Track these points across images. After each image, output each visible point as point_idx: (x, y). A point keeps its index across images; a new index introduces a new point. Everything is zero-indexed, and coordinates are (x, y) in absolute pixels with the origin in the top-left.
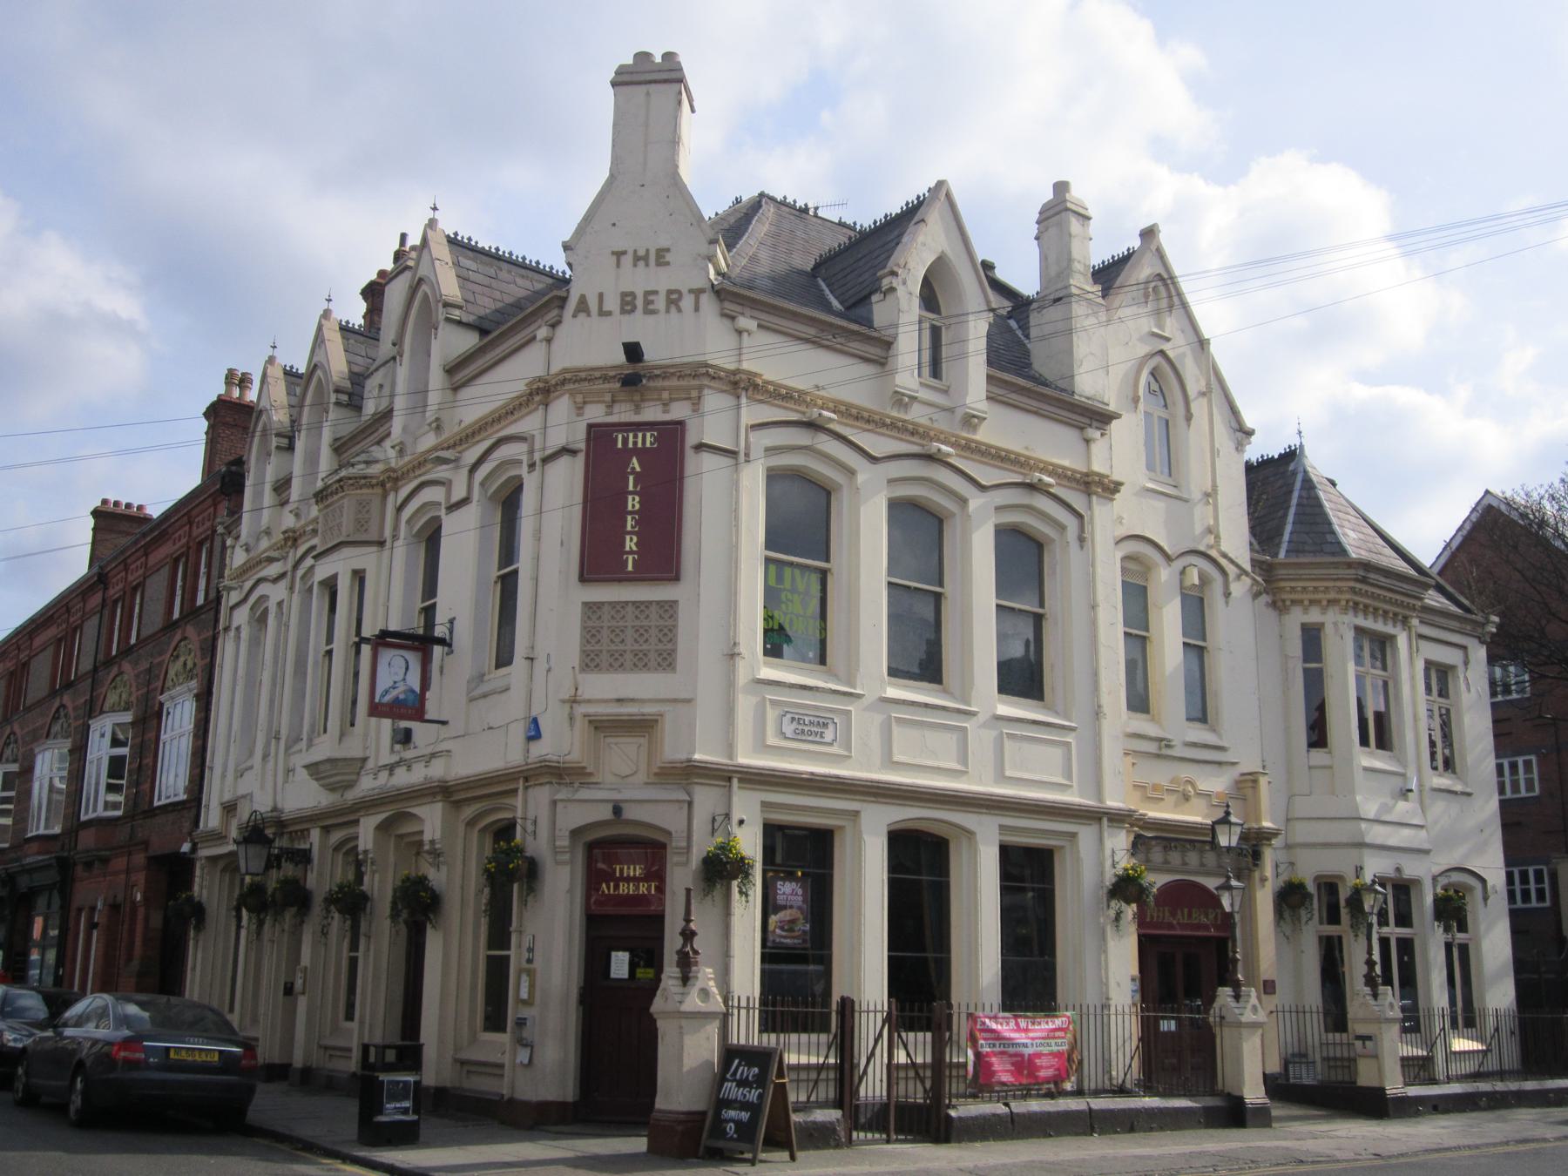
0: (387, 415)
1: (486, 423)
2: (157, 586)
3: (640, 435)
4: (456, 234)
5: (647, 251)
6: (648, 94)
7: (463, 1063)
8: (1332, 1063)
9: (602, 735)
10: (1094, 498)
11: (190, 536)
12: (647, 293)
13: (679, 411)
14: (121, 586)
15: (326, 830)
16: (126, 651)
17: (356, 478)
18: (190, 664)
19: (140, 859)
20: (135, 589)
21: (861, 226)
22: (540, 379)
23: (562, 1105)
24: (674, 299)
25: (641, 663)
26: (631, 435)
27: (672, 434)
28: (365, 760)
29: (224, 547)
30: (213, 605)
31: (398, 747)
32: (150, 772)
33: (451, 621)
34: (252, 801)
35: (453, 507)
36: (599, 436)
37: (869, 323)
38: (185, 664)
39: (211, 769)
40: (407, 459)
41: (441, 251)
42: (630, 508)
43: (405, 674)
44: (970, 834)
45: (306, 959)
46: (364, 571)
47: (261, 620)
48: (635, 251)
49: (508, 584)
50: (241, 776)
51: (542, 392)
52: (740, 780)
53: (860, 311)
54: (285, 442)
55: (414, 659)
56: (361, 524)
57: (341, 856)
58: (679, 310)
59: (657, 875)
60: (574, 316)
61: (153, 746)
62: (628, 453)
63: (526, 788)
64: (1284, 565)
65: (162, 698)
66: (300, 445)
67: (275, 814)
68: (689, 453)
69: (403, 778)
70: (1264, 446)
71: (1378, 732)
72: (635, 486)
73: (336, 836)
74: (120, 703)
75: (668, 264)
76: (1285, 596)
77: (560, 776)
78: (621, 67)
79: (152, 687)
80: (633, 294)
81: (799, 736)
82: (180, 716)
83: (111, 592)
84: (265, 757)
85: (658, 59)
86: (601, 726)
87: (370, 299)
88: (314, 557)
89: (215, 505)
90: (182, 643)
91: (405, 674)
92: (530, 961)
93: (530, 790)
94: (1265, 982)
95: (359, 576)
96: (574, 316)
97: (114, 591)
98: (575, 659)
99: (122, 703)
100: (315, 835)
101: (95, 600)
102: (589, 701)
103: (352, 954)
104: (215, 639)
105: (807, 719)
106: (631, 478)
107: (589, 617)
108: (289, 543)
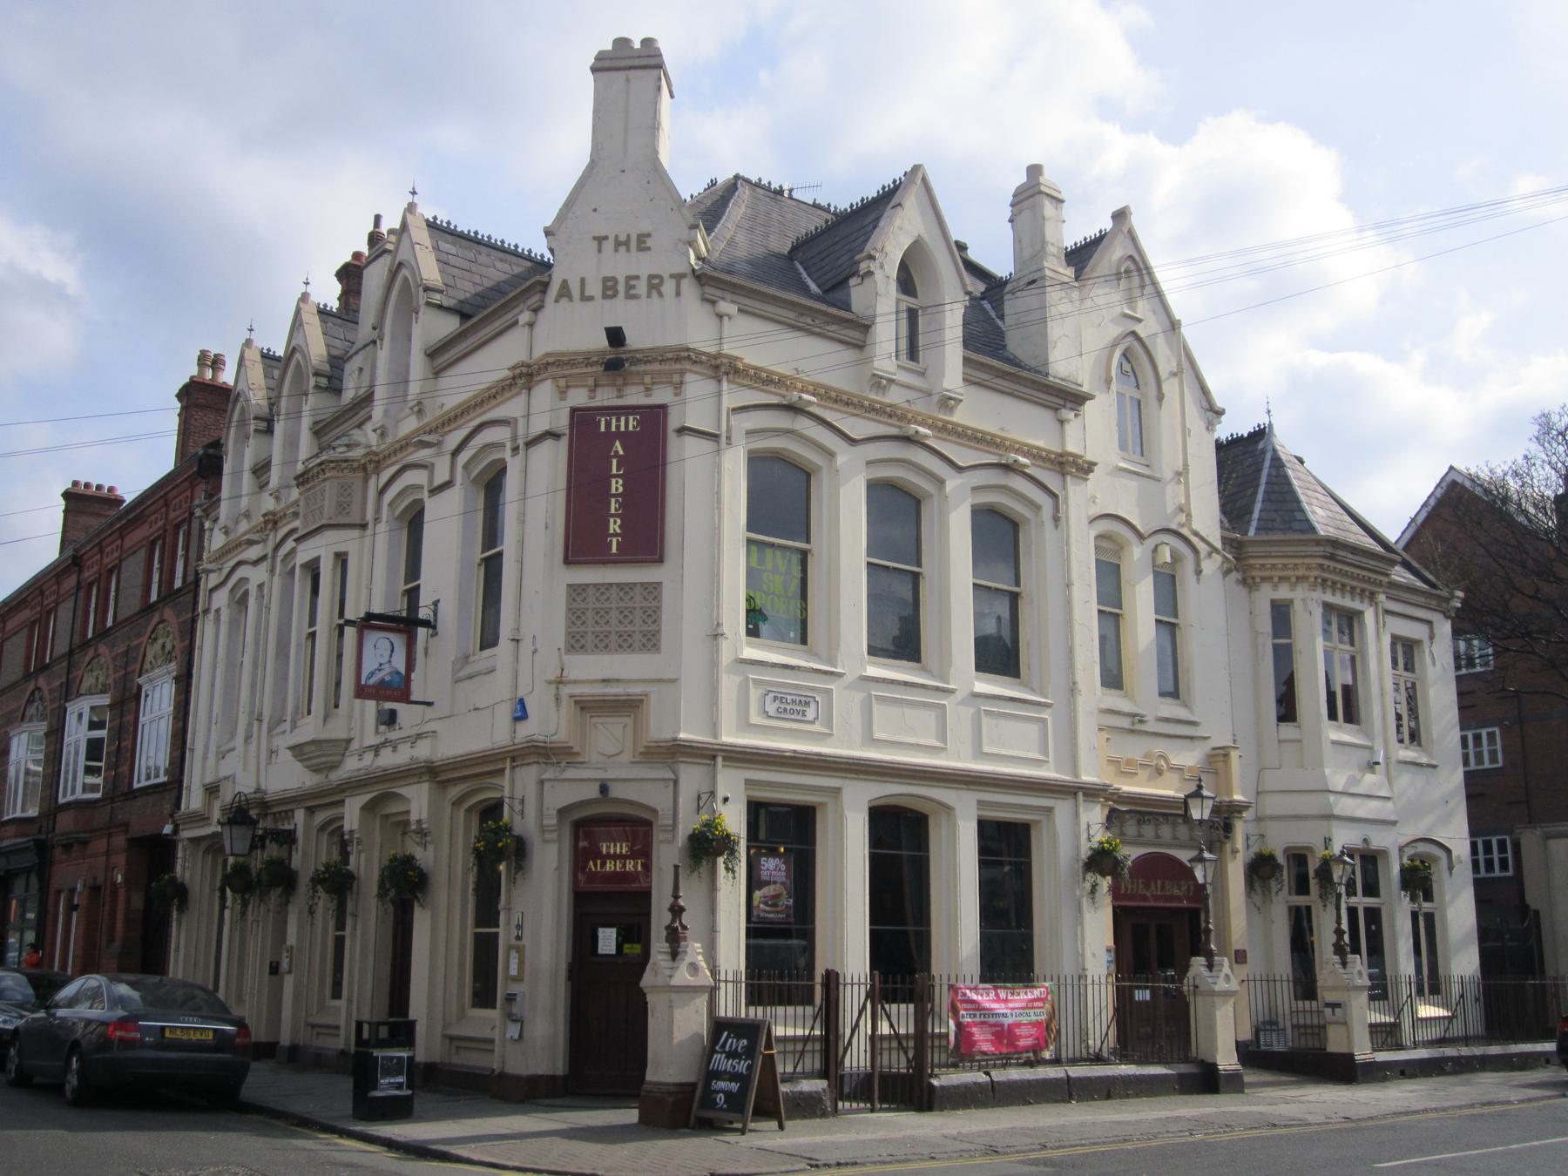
0: (367, 399)
1: (469, 407)
2: (133, 568)
3: (623, 419)
4: (435, 218)
5: (629, 236)
6: (628, 80)
7: (452, 1039)
8: (1302, 1030)
9: (588, 715)
10: (1069, 478)
11: (166, 519)
12: (629, 278)
13: (661, 396)
14: (96, 568)
15: (311, 811)
16: (103, 634)
17: (337, 461)
18: (168, 647)
19: (120, 841)
20: (111, 571)
21: (836, 208)
22: (523, 365)
23: (552, 1079)
24: (655, 283)
25: (626, 644)
26: (614, 421)
27: (654, 417)
28: (349, 741)
29: (202, 530)
30: (192, 587)
31: (382, 728)
32: (129, 754)
33: (436, 603)
34: (234, 782)
35: (436, 490)
36: (582, 419)
37: (847, 307)
38: (163, 646)
39: (192, 750)
40: (389, 440)
41: (421, 235)
42: (613, 491)
43: (391, 656)
44: (949, 809)
45: (291, 939)
46: (346, 554)
47: (241, 602)
48: (617, 236)
49: (492, 567)
50: (223, 757)
51: (525, 377)
52: (725, 759)
53: (837, 295)
54: (265, 424)
55: (399, 641)
56: (343, 507)
57: (325, 837)
58: (661, 295)
59: (644, 853)
60: (557, 301)
61: (131, 729)
62: (610, 437)
63: (513, 768)
64: (1253, 543)
65: (140, 681)
66: (279, 428)
67: (258, 795)
68: (671, 436)
69: (388, 759)
70: (1235, 425)
71: (1346, 706)
72: (618, 470)
73: (321, 817)
74: (97, 686)
75: (649, 249)
76: (1253, 574)
77: (547, 756)
78: (601, 53)
79: (129, 669)
80: (614, 280)
81: (782, 714)
82: (159, 699)
83: (86, 574)
84: (248, 738)
85: (637, 45)
86: (587, 707)
87: (345, 282)
88: (295, 540)
89: (192, 488)
90: (161, 626)
91: (391, 656)
92: (519, 938)
93: (517, 770)
94: (1237, 952)
95: (341, 559)
96: (557, 301)
97: (89, 574)
98: (560, 639)
99: (100, 686)
100: (300, 816)
101: (70, 582)
102: (575, 682)
103: (338, 933)
104: (194, 621)
105: (789, 698)
106: (614, 462)
107: (574, 599)
108: (270, 526)
